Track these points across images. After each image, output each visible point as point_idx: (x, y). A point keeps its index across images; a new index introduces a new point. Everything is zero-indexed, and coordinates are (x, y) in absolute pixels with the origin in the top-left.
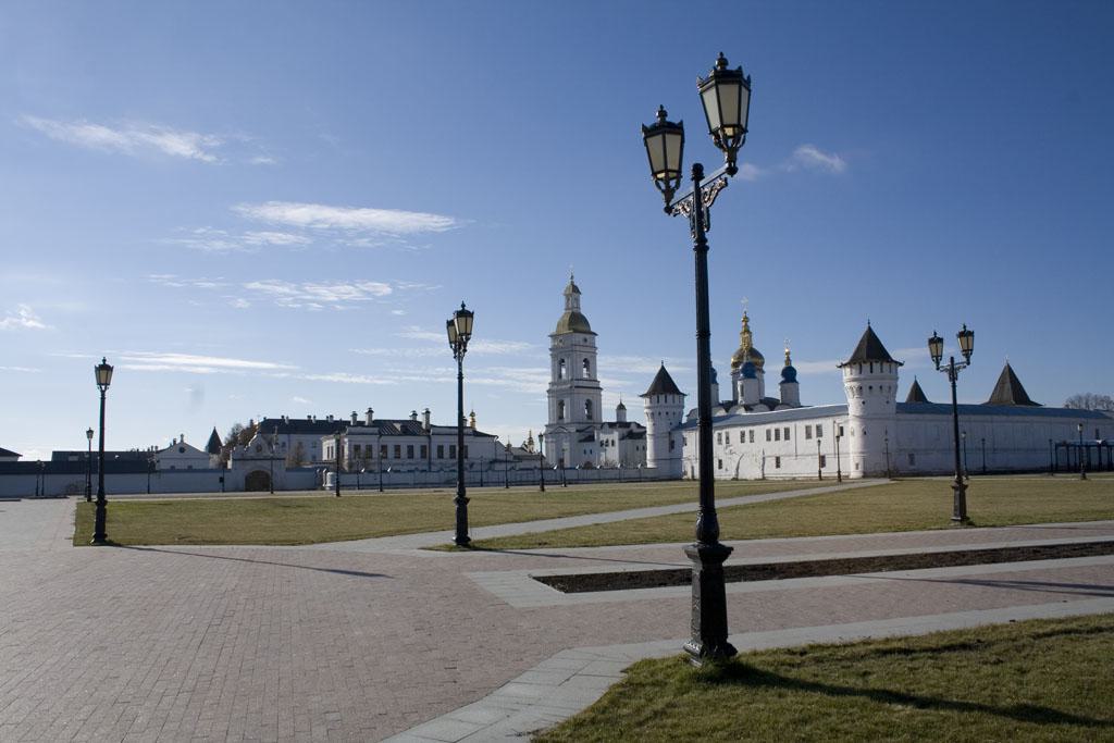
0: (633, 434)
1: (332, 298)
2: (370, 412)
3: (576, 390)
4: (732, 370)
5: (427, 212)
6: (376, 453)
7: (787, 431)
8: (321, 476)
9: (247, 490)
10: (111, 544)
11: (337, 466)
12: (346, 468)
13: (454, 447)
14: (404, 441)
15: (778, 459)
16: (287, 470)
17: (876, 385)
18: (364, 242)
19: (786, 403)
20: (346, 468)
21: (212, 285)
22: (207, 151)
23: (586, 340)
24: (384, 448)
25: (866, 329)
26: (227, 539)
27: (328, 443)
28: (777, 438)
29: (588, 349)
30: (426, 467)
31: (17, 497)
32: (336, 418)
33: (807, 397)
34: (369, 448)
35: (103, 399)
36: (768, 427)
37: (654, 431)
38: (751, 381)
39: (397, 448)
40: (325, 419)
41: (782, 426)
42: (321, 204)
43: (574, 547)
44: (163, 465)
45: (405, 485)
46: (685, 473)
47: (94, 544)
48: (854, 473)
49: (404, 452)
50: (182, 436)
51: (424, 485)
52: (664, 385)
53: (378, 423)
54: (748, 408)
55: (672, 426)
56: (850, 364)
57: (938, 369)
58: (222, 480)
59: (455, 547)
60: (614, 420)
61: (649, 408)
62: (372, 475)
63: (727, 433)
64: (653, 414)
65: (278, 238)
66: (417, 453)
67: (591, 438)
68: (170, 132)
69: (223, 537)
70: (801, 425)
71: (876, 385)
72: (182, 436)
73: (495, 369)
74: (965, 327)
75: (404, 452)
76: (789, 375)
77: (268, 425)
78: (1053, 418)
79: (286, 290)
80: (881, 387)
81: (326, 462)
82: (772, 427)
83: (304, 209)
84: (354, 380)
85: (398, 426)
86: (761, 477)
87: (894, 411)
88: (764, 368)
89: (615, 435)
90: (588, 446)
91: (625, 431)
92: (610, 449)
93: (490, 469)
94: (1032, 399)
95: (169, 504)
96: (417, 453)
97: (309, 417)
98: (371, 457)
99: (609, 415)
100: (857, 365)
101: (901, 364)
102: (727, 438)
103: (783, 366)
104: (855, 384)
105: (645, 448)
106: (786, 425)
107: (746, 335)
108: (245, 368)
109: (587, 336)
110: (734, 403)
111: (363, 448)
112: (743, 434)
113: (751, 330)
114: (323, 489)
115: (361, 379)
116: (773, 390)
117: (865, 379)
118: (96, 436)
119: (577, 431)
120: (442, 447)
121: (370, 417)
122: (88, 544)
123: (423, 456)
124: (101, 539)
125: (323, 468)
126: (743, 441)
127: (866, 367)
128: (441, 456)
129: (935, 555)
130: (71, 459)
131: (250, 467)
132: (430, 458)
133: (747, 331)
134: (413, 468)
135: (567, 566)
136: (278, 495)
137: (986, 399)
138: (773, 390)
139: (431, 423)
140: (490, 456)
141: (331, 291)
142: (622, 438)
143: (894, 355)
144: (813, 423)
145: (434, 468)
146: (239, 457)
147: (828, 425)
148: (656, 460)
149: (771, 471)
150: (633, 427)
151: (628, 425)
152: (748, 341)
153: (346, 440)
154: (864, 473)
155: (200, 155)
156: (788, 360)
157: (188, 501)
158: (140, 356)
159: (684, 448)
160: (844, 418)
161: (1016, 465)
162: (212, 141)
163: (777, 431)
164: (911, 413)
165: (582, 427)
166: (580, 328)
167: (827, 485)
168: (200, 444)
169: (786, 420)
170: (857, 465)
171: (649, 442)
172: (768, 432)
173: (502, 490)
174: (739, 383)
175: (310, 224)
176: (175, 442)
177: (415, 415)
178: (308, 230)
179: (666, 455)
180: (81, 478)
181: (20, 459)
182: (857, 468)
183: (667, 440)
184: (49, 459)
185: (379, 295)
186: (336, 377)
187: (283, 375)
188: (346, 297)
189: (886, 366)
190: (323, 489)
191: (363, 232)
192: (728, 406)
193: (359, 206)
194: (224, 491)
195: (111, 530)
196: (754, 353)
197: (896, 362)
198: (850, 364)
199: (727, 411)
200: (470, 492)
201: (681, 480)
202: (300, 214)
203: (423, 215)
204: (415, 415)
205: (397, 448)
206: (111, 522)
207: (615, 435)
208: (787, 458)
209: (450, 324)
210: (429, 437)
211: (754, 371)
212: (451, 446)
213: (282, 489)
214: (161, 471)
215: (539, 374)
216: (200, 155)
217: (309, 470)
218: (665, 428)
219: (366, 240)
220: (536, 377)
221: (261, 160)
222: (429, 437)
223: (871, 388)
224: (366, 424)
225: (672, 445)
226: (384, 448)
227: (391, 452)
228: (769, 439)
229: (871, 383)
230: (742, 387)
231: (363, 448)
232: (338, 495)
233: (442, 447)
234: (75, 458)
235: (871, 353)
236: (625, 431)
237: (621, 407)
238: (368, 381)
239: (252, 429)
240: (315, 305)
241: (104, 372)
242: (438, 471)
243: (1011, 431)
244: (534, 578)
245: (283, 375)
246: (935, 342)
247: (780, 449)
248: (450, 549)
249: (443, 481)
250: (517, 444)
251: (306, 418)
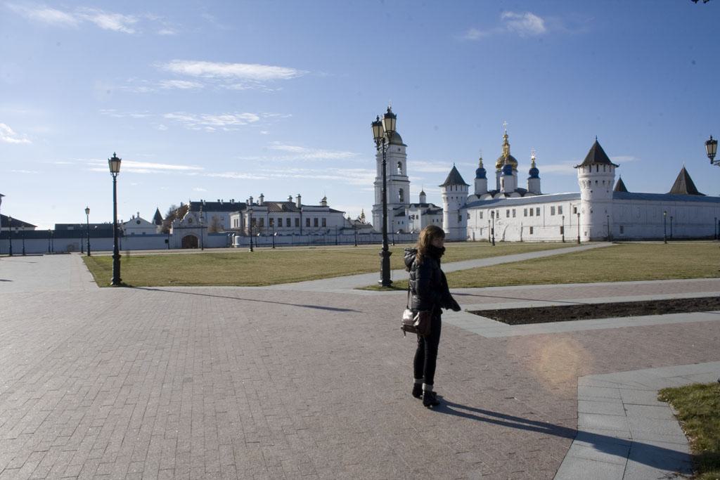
0: (431, 211)
1: (220, 123)
2: (262, 196)
3: (393, 183)
4: (496, 169)
5: (278, 66)
6: (266, 223)
7: (538, 210)
8: (231, 238)
9: (183, 248)
10: (124, 285)
11: (240, 232)
12: (247, 233)
14: (285, 216)
15: (531, 229)
16: (209, 234)
17: (600, 179)
18: (237, 86)
19: (533, 191)
20: (247, 233)
21: (143, 116)
22: (129, 26)
23: (399, 150)
24: (271, 220)
25: (594, 142)
26: (206, 282)
27: (235, 217)
28: (531, 214)
29: (402, 156)
30: (299, 233)
31: (39, 253)
32: (236, 201)
33: (546, 188)
34: (262, 220)
35: (115, 182)
36: (525, 207)
37: (449, 209)
38: (509, 177)
39: (280, 220)
40: (229, 201)
41: (535, 207)
42: (207, 61)
43: (467, 287)
44: (128, 232)
45: (286, 244)
46: (469, 237)
47: (113, 286)
48: (583, 239)
49: (284, 223)
50: (138, 213)
51: (299, 244)
52: (455, 179)
53: (267, 204)
54: (507, 195)
55: (461, 206)
56: (583, 165)
57: (712, 163)
58: (167, 241)
60: (418, 202)
61: (445, 194)
62: (265, 238)
63: (497, 211)
64: (447, 198)
65: (182, 84)
66: (293, 222)
67: (403, 214)
68: (102, 13)
69: (201, 280)
70: (548, 206)
71: (600, 179)
72: (138, 213)
73: (331, 169)
74: (711, 137)
75: (284, 223)
76: (534, 173)
77: (196, 206)
78: (716, 204)
79: (191, 119)
80: (604, 182)
81: (233, 230)
82: (528, 207)
83: (196, 65)
84: (240, 177)
85: (280, 206)
86: (520, 240)
87: (612, 197)
88: (518, 169)
89: (419, 212)
90: (401, 219)
91: (425, 209)
92: (415, 220)
93: (341, 233)
94: (699, 191)
95: (143, 257)
96: (293, 222)
97: (219, 200)
98: (263, 226)
99: (414, 198)
100: (588, 166)
101: (617, 166)
102: (498, 214)
103: (530, 167)
104: (586, 179)
105: (442, 221)
106: (538, 206)
107: (507, 147)
108: (168, 170)
109: (400, 147)
110: (498, 191)
111: (258, 220)
112: (508, 212)
113: (509, 143)
114: (233, 247)
115: (244, 176)
116: (523, 183)
117: (593, 176)
119: (394, 209)
120: (281, 219)
121: (262, 200)
122: (109, 286)
123: (297, 225)
124: (118, 282)
125: (232, 234)
126: (508, 216)
127: (594, 168)
128: (308, 225)
130: (69, 228)
131: (185, 233)
132: (301, 226)
133: (507, 144)
134: (291, 233)
135: (477, 302)
136: (207, 251)
137: (668, 191)
138: (523, 183)
139: (302, 203)
140: (340, 225)
141: (220, 119)
142: (423, 214)
143: (613, 160)
144: (556, 205)
145: (304, 233)
146: (178, 226)
147: (566, 206)
148: (450, 228)
149: (527, 237)
150: (430, 207)
151: (427, 205)
152: (507, 151)
153: (247, 215)
154: (590, 238)
155: (124, 29)
156: (534, 164)
157: (155, 255)
158: (101, 162)
159: (468, 220)
160: (577, 201)
161: (690, 234)
162: (131, 20)
163: (532, 210)
164: (622, 199)
165: (398, 206)
166: (396, 141)
167: (568, 246)
168: (149, 218)
169: (538, 203)
170: (586, 233)
171: (445, 216)
172: (525, 210)
173: (351, 248)
174: (501, 178)
175: (202, 75)
176: (133, 217)
177: (291, 198)
178: (200, 78)
179: (456, 225)
180: (78, 241)
181: (36, 229)
182: (586, 235)
183: (457, 216)
184: (53, 228)
185: (250, 121)
186: (228, 175)
187: (194, 174)
188: (230, 123)
189: (607, 167)
190: (233, 247)
191: (236, 79)
192: (493, 193)
193: (233, 61)
194: (169, 249)
195: (124, 276)
196: (511, 159)
197: (614, 165)
198: (583, 165)
199: (493, 196)
200: (391, 247)
201: (465, 241)
202: (194, 68)
203: (275, 68)
204: (291, 198)
205: (280, 220)
207: (419, 212)
208: (538, 228)
209: (377, 124)
210: (301, 213)
211: (511, 171)
212: (323, 219)
214: (126, 236)
215: (359, 172)
216: (124, 29)
217: (222, 234)
218: (456, 208)
219: (239, 85)
220: (358, 175)
221: (165, 32)
222: (301, 213)
223: (597, 182)
224: (260, 204)
225: (460, 218)
226: (271, 220)
227: (276, 223)
228: (526, 215)
229: (597, 179)
230: (503, 181)
231: (258, 220)
232: (252, 250)
233: (281, 219)
234: (72, 228)
235: (598, 158)
236: (425, 209)
237: (423, 194)
238: (249, 177)
239: (183, 209)
240: (211, 128)
241: (115, 162)
242: (307, 235)
243: (685, 211)
244: (469, 312)
245: (194, 174)
246: (712, 144)
247: (533, 222)
248: (379, 289)
249: (310, 241)
250: (354, 218)
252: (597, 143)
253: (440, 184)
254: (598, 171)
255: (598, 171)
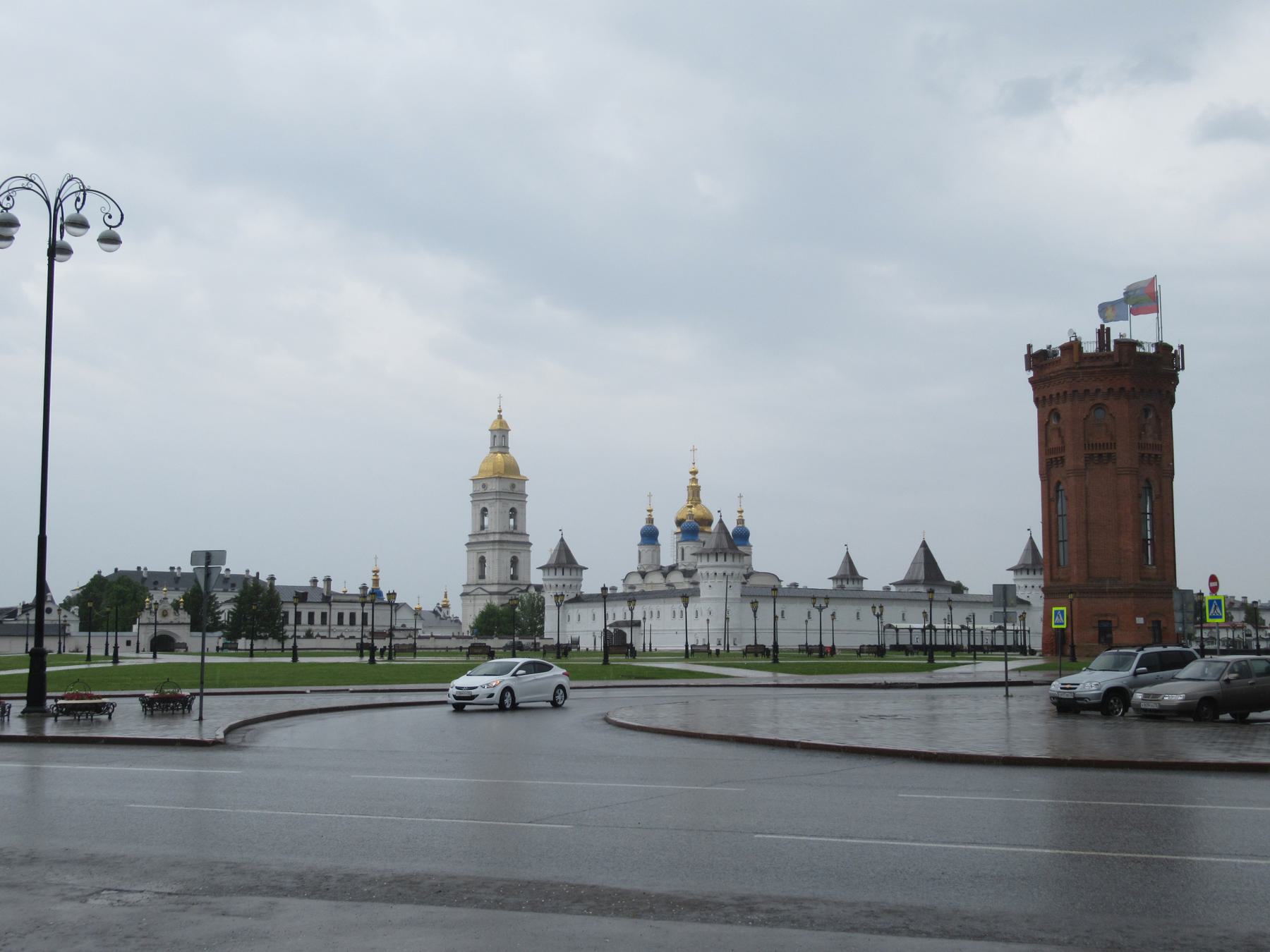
13: (326, 613)
25: (1027, 539)
30: (326, 634)
59: (550, 708)
97: (172, 568)
110: (673, 568)
117: (548, 580)
118: (728, 586)
128: (340, 622)
129: (1024, 682)
145: (333, 635)
206: (721, 629)
213: (257, 657)
242: (338, 638)
251: (244, 573)
252: (562, 540)
253: (538, 567)
254: (563, 574)
255: (563, 574)
